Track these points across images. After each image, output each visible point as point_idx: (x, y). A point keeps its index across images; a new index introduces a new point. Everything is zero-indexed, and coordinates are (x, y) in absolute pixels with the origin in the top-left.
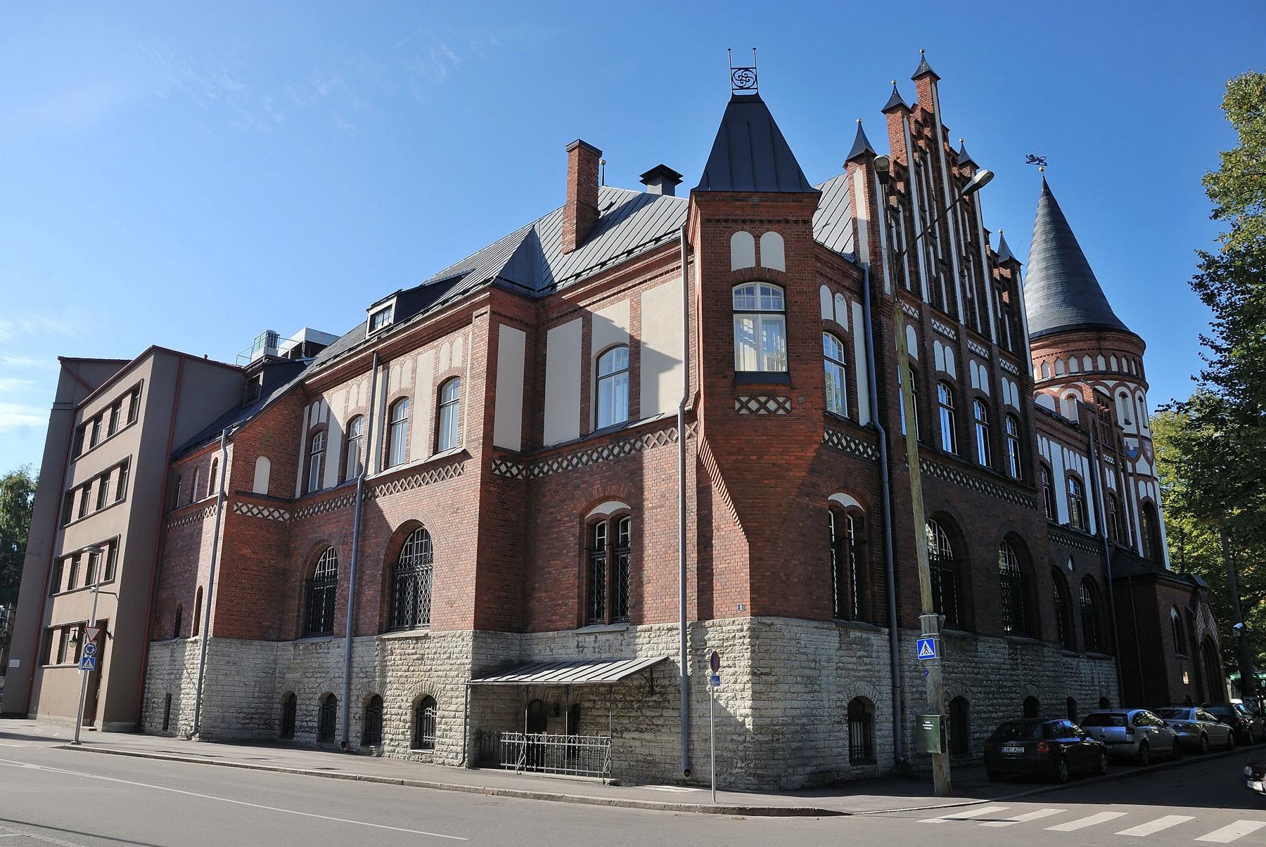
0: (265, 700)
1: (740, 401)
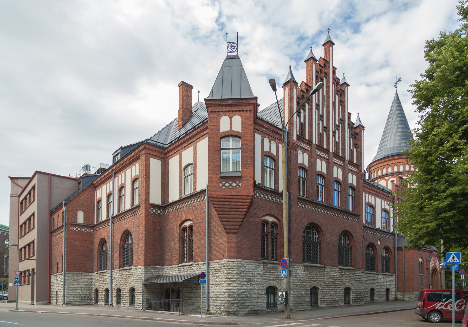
0: (89, 292)
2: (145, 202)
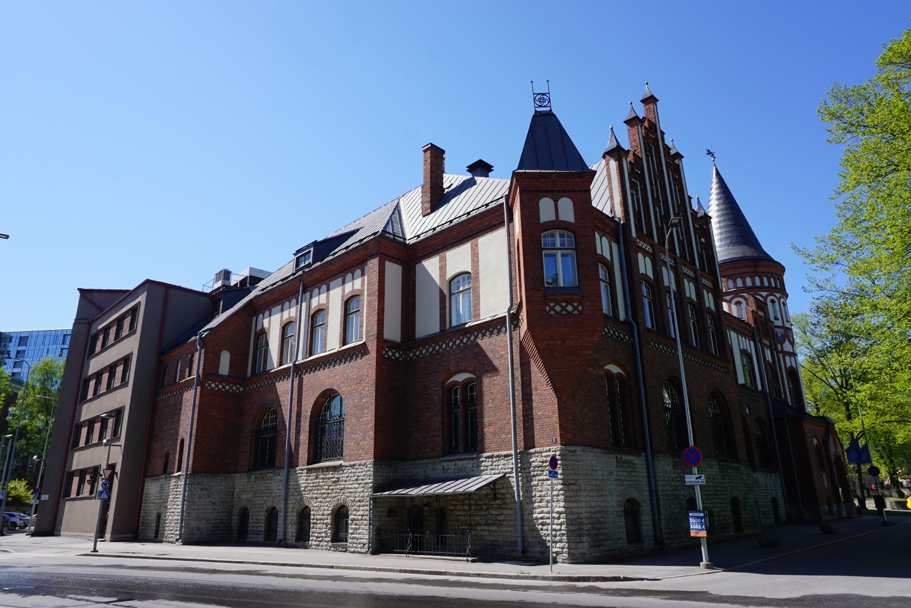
1: (549, 306)
2: (377, 338)
